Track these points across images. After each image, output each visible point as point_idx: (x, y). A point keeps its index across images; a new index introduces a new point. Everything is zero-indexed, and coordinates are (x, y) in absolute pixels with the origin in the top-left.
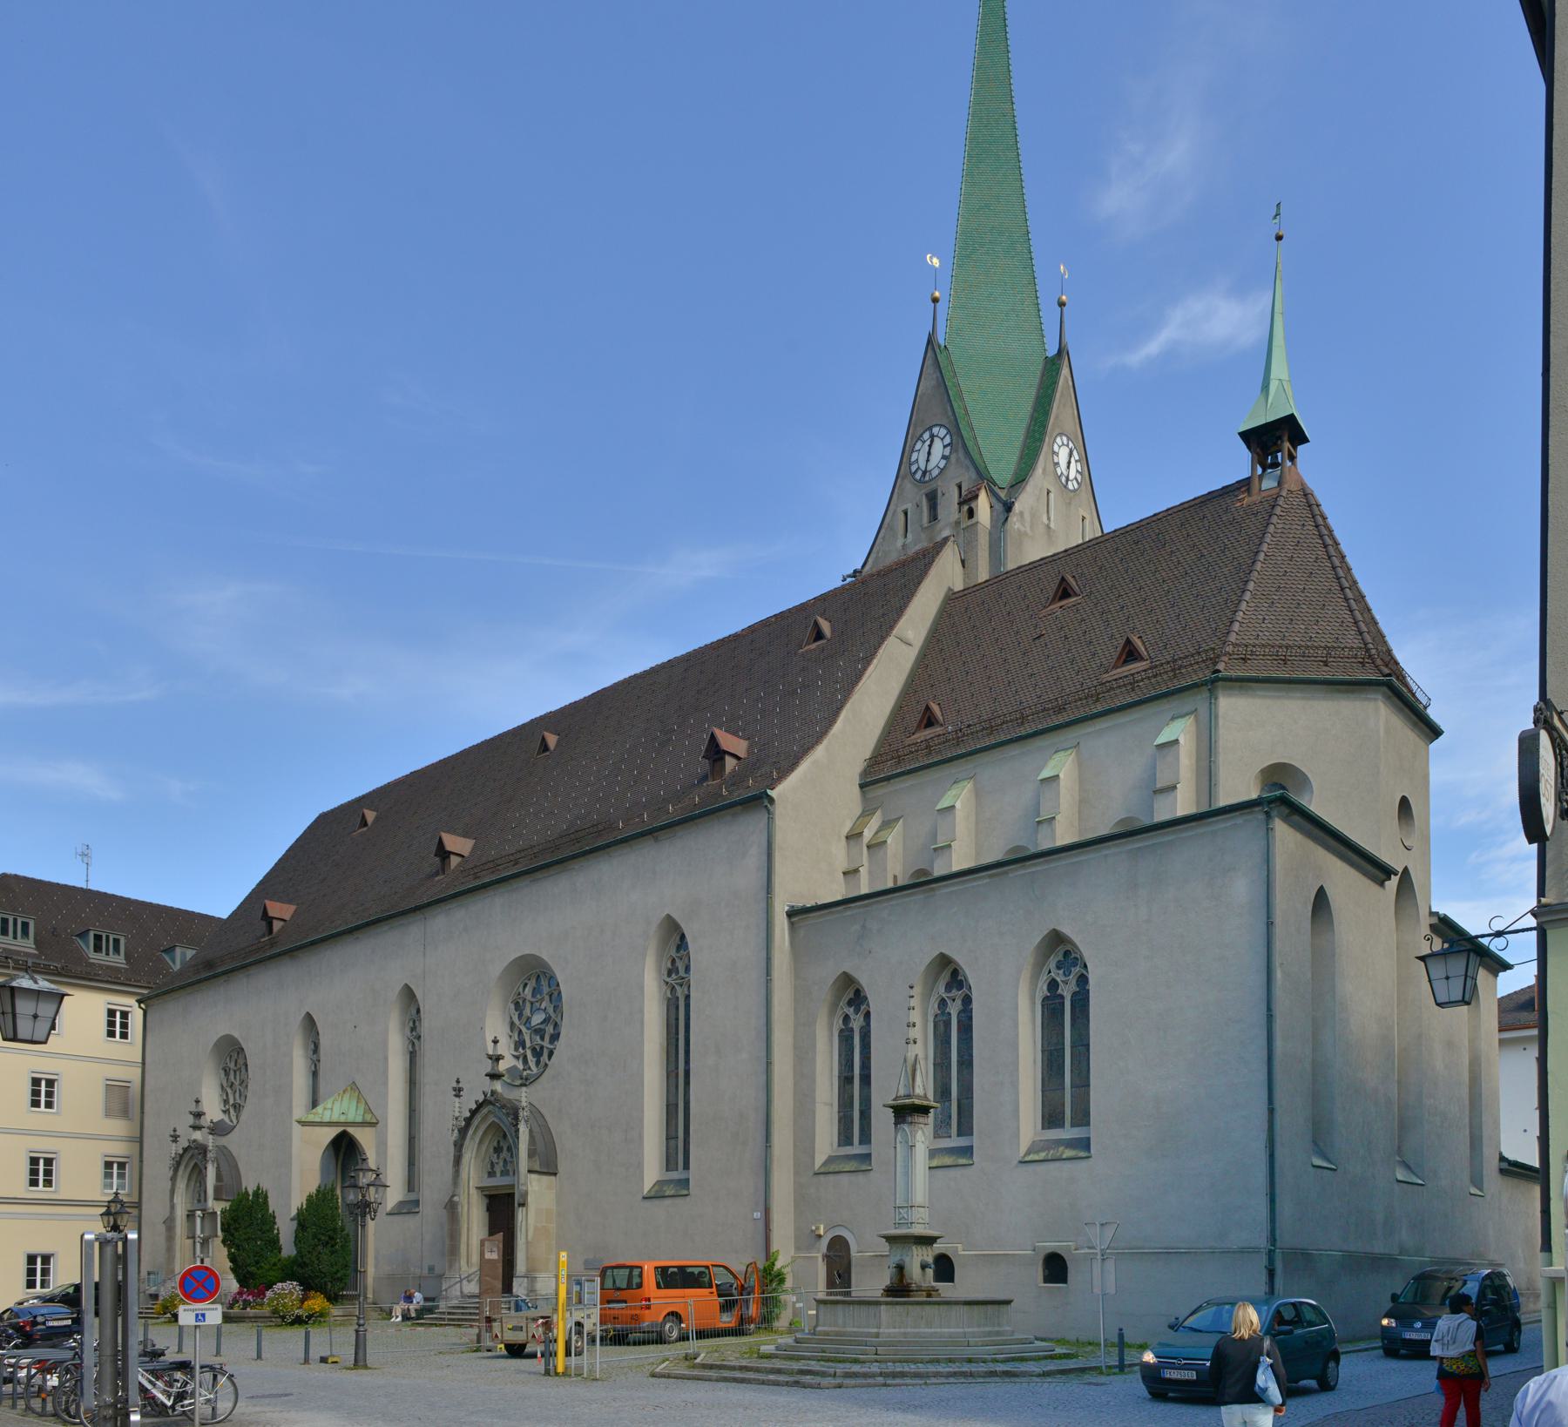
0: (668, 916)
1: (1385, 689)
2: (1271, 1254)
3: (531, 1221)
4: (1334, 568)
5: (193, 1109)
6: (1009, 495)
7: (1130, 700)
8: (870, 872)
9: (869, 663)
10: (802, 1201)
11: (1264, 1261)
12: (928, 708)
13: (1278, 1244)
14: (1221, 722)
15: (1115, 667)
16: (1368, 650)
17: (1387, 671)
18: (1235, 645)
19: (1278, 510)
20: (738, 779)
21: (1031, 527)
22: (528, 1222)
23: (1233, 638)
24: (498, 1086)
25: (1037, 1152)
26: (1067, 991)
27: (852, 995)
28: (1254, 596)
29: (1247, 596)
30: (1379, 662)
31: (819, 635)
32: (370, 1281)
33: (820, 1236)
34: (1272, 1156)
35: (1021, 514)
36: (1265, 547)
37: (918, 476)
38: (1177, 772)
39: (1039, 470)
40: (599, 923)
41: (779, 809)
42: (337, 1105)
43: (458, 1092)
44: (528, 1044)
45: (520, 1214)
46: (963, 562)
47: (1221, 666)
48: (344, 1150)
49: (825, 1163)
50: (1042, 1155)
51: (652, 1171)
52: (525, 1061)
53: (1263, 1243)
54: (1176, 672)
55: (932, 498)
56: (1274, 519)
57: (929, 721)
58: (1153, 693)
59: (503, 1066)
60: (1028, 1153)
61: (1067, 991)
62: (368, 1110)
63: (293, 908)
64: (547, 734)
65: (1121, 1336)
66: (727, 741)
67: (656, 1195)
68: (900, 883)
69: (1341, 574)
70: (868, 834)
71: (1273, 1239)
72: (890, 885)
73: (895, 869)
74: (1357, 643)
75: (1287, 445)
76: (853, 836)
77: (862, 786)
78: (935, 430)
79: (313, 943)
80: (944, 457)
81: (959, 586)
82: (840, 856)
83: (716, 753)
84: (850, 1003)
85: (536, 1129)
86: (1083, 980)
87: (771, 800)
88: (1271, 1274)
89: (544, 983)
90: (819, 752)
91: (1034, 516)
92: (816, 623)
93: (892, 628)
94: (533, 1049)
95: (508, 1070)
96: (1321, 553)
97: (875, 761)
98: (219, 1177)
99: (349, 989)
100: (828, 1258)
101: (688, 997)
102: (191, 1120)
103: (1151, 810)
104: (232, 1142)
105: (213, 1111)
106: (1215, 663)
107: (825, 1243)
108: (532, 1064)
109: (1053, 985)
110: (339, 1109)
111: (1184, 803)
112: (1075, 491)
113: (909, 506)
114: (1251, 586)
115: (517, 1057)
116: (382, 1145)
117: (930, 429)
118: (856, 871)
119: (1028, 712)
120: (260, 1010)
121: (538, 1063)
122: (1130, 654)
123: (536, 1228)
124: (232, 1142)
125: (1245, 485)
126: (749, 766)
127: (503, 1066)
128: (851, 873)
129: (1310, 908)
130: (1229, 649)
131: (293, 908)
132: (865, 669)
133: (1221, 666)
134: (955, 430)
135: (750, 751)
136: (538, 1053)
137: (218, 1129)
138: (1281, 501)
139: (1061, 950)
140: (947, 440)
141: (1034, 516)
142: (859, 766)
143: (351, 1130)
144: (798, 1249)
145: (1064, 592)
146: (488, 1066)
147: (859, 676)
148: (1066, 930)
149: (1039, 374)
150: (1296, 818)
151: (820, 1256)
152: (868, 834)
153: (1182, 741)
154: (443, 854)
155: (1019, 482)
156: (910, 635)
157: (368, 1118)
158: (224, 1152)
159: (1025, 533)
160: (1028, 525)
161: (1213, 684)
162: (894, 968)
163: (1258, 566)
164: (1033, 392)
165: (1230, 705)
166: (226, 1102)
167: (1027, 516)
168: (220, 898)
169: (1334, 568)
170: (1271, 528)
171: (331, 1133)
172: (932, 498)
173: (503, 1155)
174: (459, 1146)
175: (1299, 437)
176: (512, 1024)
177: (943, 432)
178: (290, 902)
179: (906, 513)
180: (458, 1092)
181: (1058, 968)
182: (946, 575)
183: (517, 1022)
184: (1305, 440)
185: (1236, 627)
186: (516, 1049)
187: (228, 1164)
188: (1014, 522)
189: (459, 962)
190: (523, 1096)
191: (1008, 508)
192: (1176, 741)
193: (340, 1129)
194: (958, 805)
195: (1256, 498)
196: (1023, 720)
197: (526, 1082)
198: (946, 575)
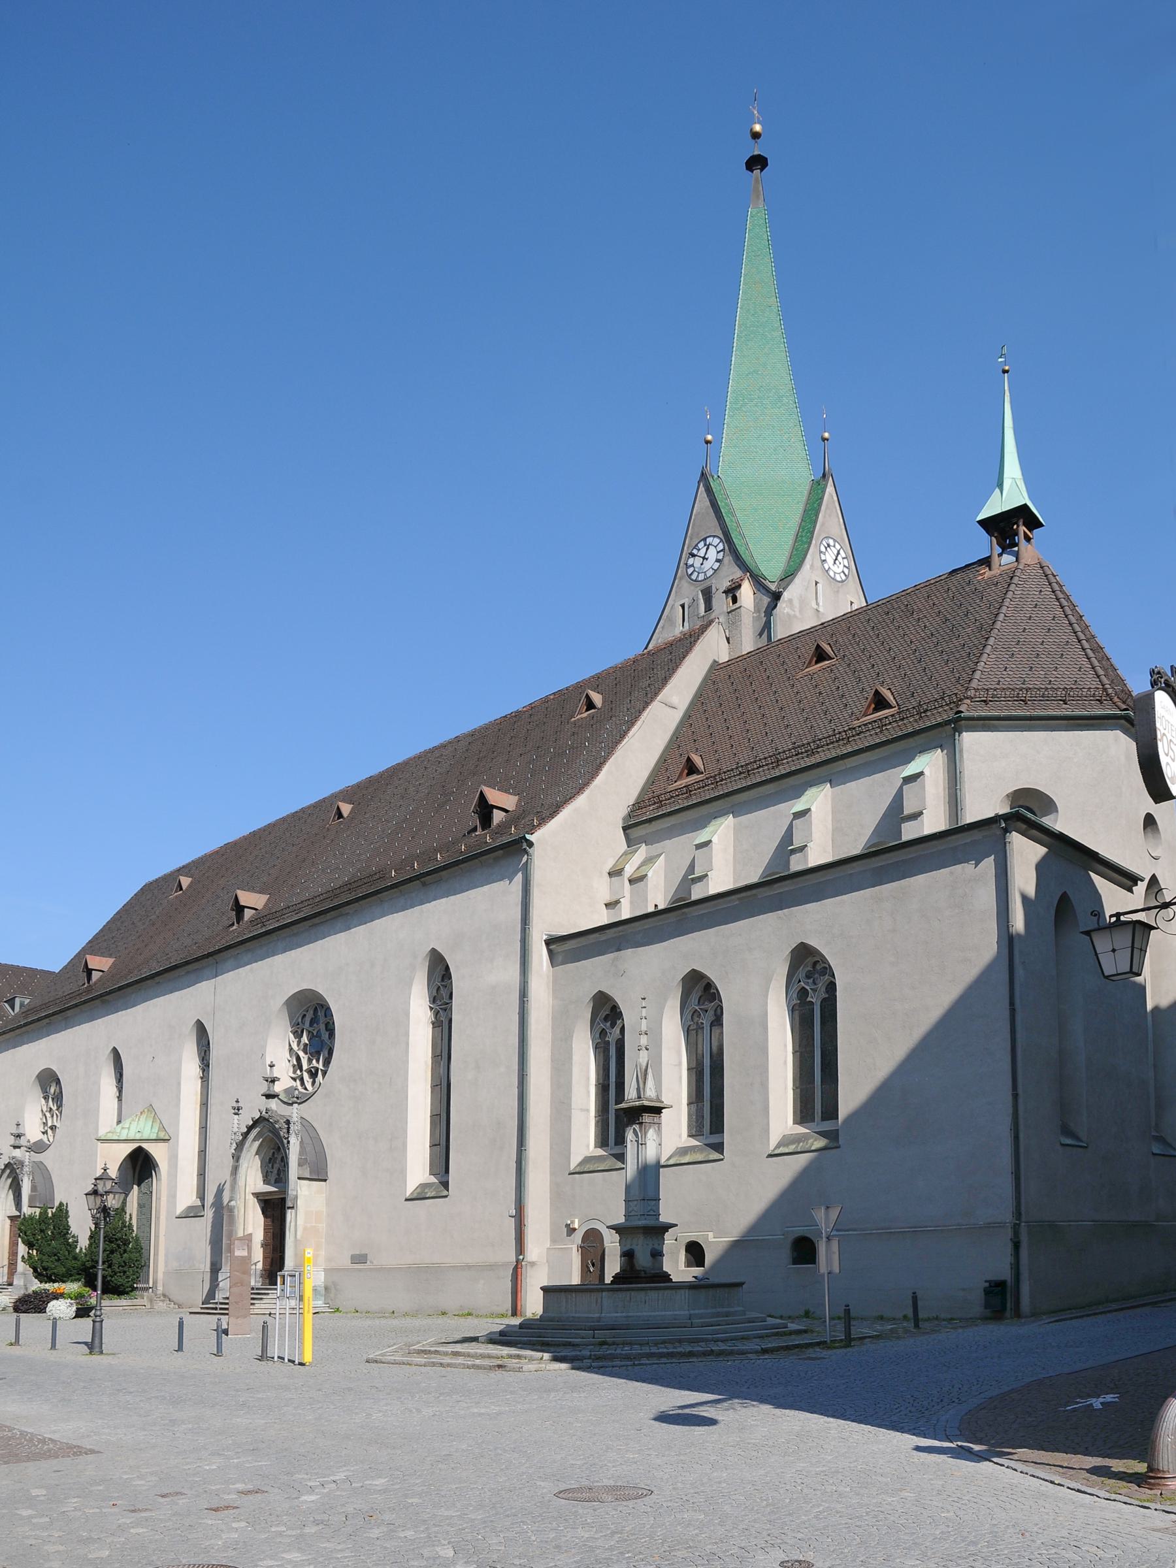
0: (434, 951)
1: (1123, 721)
2: (1016, 1228)
3: (300, 1222)
4: (1071, 624)
5: (15, 1131)
6: (778, 586)
7: (878, 741)
8: (631, 902)
9: (633, 724)
10: (557, 1196)
11: (1009, 1233)
12: (689, 759)
13: (1023, 1219)
14: (965, 756)
15: (865, 715)
16: (1105, 690)
17: (1124, 707)
18: (976, 690)
19: (1015, 580)
20: (505, 826)
21: (801, 611)
22: (296, 1223)
23: (974, 684)
24: (273, 1104)
25: (787, 1145)
26: (815, 999)
27: (606, 1013)
28: (994, 649)
29: (988, 649)
30: (1116, 699)
31: (590, 705)
32: (160, 1275)
33: (575, 1230)
34: (1016, 1138)
35: (790, 601)
36: (1004, 610)
37: (694, 577)
38: (923, 799)
39: (807, 566)
40: (367, 964)
41: (537, 853)
42: (134, 1125)
43: (237, 1110)
44: (305, 1066)
45: (289, 1215)
46: (728, 640)
47: (963, 708)
48: (140, 1165)
49: (580, 1164)
50: (791, 1148)
51: (418, 1172)
52: (303, 1083)
53: (1008, 1217)
54: (922, 712)
55: (707, 594)
56: (1012, 587)
57: (691, 769)
58: (900, 734)
59: (278, 1088)
60: (778, 1147)
61: (815, 999)
62: (163, 1128)
63: (111, 961)
64: (341, 804)
65: (847, 1312)
66: (494, 796)
67: (419, 1196)
68: (660, 908)
69: (1073, 620)
70: (629, 870)
71: (1018, 1214)
72: (651, 909)
73: (657, 896)
74: (1095, 684)
75: (1022, 529)
76: (616, 873)
77: (625, 829)
78: (709, 540)
79: (120, 988)
80: (718, 561)
81: (724, 658)
82: (603, 889)
83: (485, 810)
84: (606, 1019)
85: (307, 1140)
86: (832, 987)
87: (531, 844)
88: (1017, 1246)
89: (321, 1014)
90: (581, 801)
91: (803, 601)
92: (587, 696)
93: (656, 694)
94: (309, 1071)
95: (286, 1091)
96: (1059, 612)
97: (638, 806)
98: (34, 1188)
99: (152, 1026)
100: (584, 1250)
101: (450, 1021)
102: (12, 1140)
103: (787, 864)
104: (46, 1158)
105: (33, 1133)
106: (958, 706)
107: (578, 1237)
108: (309, 1085)
109: (803, 993)
110: (139, 1129)
111: (934, 821)
112: (843, 581)
113: (686, 601)
114: (991, 641)
115: (294, 1079)
116: (173, 1158)
117: (705, 539)
118: (617, 902)
119: (783, 756)
120: (73, 1048)
121: (313, 1083)
122: (880, 703)
123: (305, 1229)
124: (46, 1158)
125: (986, 562)
126: (514, 818)
127: (278, 1088)
128: (611, 905)
129: (1053, 912)
130: (971, 693)
131: (111, 961)
132: (629, 729)
133: (963, 708)
134: (727, 539)
135: (518, 805)
136: (313, 1074)
137: (39, 1147)
138: (1018, 573)
139: (810, 960)
140: (721, 547)
141: (803, 601)
142: (623, 811)
143: (145, 1146)
144: (553, 1241)
145: (820, 656)
146: (264, 1088)
147: (623, 736)
148: (813, 942)
149: (806, 493)
150: (1034, 832)
151: (575, 1248)
152: (629, 870)
153: (927, 772)
154: (239, 909)
155: (789, 576)
156: (675, 700)
157: (162, 1135)
158: (40, 1168)
159: (795, 616)
160: (797, 610)
161: (959, 723)
162: (647, 984)
163: (998, 625)
164: (801, 507)
165: (970, 740)
166: (45, 1124)
167: (796, 603)
168: (52, 956)
169: (1071, 624)
170: (1010, 594)
171: (129, 1148)
172: (707, 594)
173: (277, 1166)
174: (236, 1157)
175: (1033, 523)
176: (291, 1049)
177: (716, 541)
178: (110, 956)
179: (683, 606)
180: (237, 1110)
181: (808, 977)
182: (713, 648)
183: (295, 1047)
184: (1039, 525)
185: (978, 675)
186: (294, 1072)
187: (42, 1174)
188: (782, 605)
189: (248, 1000)
190: (294, 1112)
191: (776, 597)
192: (921, 774)
193: (135, 1145)
194: (715, 840)
195: (996, 571)
196: (778, 763)
197: (301, 1100)
198: (713, 648)
